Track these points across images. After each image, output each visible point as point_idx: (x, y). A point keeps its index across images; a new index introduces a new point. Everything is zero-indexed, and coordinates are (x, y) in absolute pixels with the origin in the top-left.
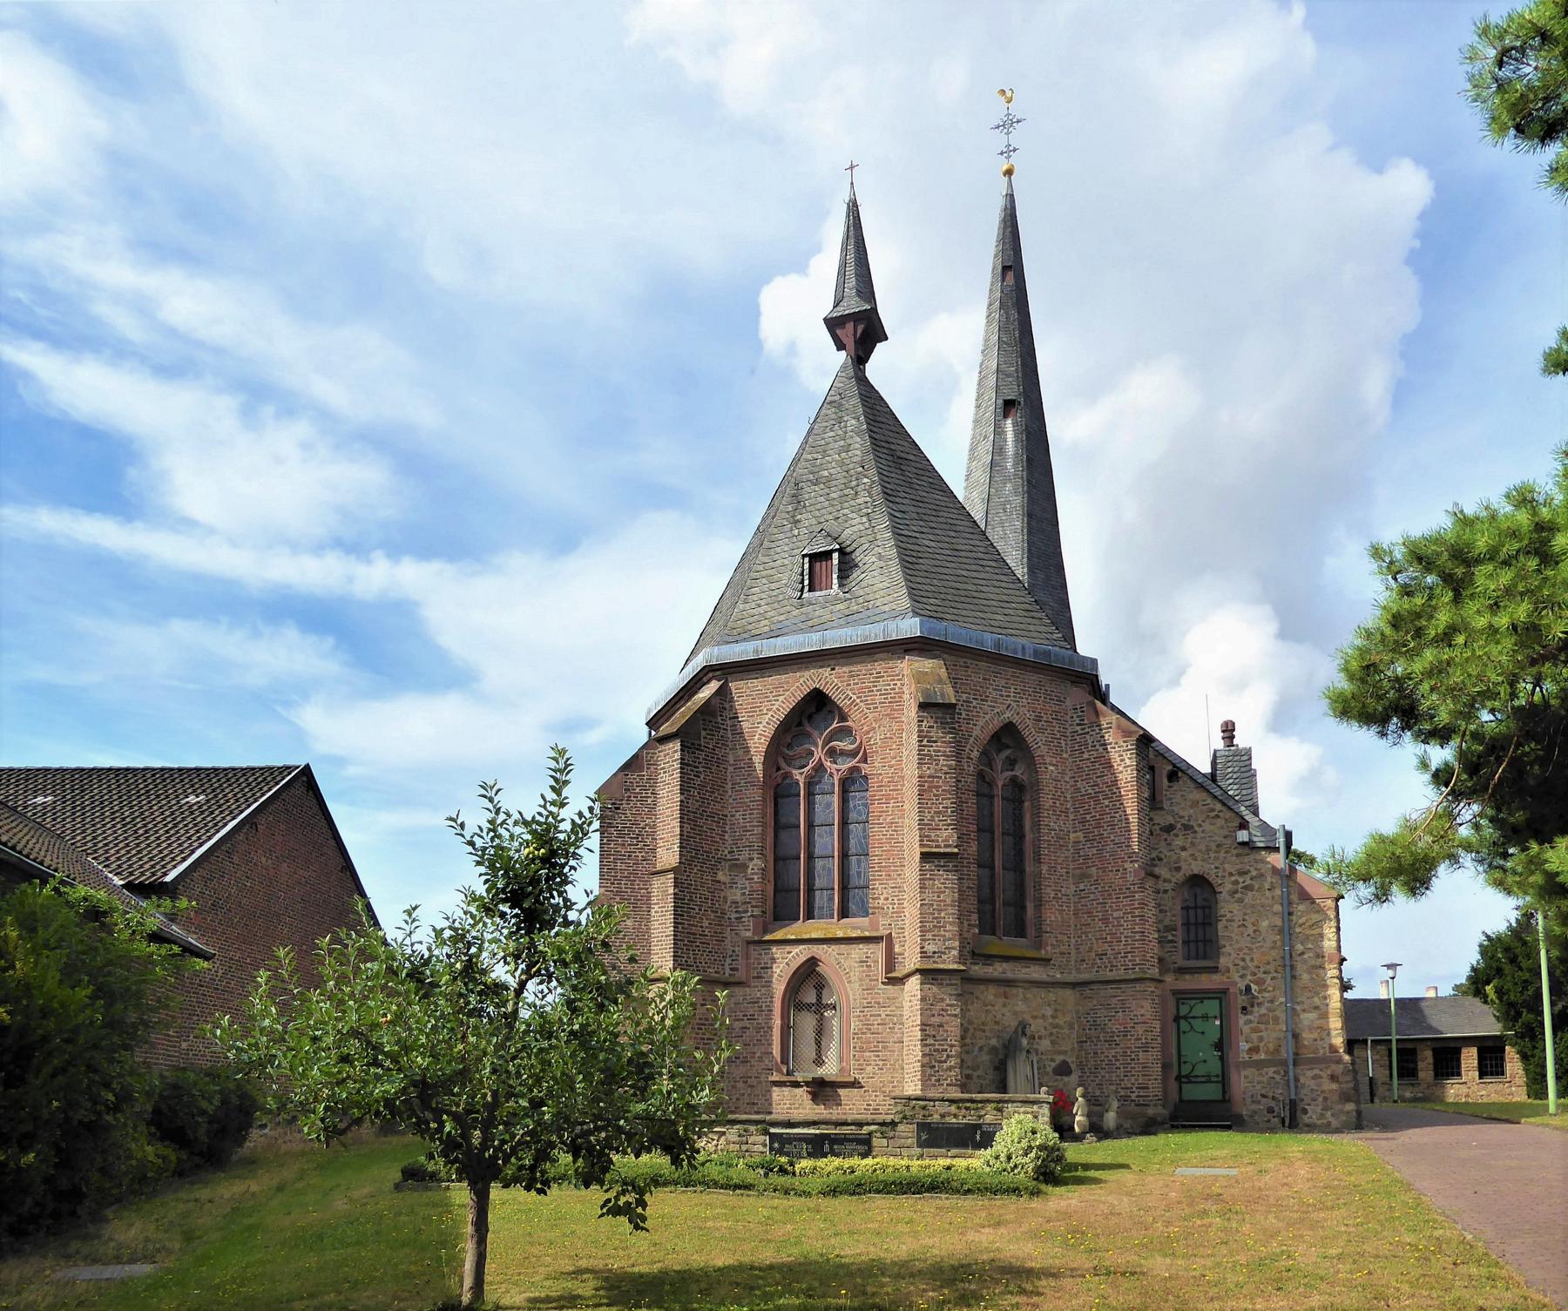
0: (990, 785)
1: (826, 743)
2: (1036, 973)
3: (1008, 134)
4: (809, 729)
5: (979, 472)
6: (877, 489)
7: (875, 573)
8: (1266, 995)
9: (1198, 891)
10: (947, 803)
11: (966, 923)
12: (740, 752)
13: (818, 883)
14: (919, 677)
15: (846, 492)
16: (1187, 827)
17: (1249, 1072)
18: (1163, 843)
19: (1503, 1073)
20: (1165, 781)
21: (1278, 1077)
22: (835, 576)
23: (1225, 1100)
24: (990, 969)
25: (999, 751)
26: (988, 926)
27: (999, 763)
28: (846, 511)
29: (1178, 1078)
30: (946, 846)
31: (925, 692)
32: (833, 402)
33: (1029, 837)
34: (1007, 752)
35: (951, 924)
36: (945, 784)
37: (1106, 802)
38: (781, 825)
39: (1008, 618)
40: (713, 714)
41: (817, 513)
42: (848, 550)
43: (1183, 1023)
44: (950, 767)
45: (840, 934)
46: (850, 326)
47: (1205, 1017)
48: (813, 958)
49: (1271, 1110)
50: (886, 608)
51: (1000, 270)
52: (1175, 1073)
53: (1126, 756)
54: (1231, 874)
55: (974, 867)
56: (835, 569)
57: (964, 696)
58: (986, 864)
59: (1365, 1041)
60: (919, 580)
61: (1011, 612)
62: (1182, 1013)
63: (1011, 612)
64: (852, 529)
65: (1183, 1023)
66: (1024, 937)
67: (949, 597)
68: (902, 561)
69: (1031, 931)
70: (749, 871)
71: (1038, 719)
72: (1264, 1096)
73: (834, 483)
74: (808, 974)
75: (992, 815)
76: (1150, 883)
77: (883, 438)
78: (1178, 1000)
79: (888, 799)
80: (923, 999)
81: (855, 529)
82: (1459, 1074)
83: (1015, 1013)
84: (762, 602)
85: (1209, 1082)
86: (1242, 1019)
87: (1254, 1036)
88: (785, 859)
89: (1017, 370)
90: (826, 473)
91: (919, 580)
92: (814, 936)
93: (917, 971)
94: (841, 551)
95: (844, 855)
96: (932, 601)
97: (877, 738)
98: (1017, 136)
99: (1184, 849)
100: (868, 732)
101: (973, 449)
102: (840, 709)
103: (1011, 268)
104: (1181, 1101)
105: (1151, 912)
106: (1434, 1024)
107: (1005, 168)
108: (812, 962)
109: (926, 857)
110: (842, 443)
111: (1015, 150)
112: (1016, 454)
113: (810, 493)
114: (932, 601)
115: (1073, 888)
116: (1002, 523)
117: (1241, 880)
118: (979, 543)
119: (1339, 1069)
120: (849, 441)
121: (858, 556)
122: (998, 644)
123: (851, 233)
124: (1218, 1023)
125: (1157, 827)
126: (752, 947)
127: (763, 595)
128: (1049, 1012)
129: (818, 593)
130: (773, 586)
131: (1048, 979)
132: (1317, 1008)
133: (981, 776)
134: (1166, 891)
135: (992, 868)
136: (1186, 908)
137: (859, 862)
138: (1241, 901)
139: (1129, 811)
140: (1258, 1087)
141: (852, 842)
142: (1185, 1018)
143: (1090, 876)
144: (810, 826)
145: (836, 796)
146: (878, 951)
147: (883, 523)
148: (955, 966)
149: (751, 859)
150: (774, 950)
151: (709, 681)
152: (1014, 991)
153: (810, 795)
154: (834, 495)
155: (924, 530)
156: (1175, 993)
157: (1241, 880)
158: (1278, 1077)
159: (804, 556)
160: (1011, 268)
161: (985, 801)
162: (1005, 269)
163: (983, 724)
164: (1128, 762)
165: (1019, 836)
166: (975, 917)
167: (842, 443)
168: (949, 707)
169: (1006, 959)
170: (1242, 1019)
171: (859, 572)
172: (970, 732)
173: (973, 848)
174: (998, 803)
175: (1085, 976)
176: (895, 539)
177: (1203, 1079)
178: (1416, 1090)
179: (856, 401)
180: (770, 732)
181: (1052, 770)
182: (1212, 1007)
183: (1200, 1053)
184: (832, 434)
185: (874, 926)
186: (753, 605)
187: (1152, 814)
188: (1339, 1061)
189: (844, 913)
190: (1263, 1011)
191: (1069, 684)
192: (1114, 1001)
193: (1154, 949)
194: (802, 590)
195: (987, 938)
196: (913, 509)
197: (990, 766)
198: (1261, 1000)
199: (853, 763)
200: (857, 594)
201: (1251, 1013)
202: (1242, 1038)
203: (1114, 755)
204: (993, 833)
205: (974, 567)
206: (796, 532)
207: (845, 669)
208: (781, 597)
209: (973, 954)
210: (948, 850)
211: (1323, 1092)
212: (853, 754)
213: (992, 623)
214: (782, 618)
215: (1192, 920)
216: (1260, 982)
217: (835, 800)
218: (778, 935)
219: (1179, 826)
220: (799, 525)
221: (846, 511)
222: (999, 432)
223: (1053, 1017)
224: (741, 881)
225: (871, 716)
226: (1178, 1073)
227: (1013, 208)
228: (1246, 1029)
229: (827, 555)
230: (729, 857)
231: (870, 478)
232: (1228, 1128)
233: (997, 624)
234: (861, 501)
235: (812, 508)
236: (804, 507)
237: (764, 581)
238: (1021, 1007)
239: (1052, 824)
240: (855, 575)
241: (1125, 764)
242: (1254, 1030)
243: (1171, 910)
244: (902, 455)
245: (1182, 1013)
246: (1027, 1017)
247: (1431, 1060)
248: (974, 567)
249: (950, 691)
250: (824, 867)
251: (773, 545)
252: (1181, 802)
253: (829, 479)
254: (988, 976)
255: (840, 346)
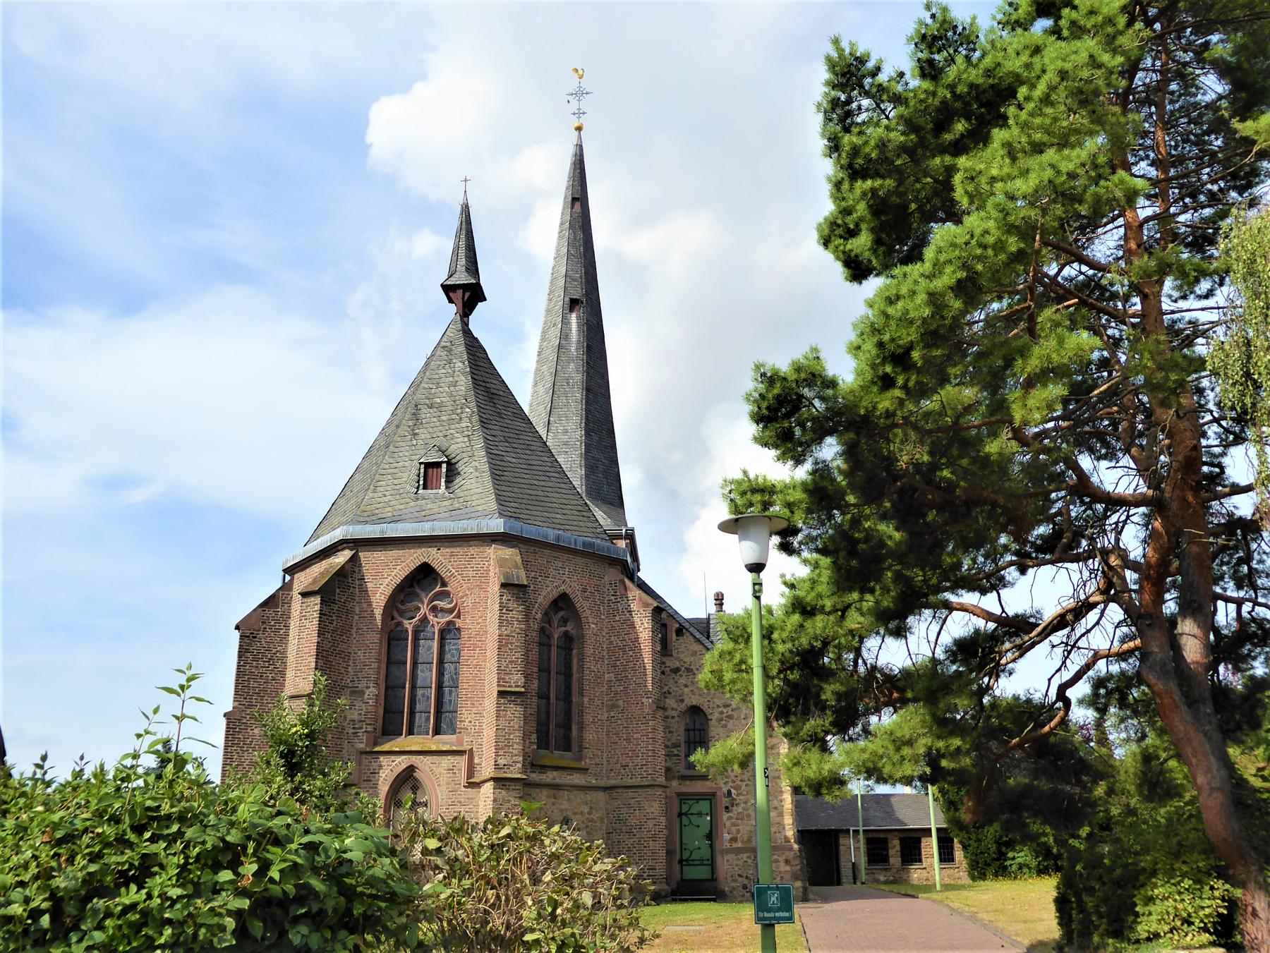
0: (549, 637)
1: (431, 601)
2: (577, 779)
3: (579, 109)
4: (418, 590)
5: (548, 352)
6: (476, 418)
7: (472, 481)
8: (742, 797)
9: (696, 717)
10: (518, 655)
11: (528, 741)
12: (365, 605)
13: (418, 708)
14: (501, 562)
15: (453, 416)
16: (688, 670)
17: (730, 857)
18: (671, 681)
19: (953, 860)
20: (674, 635)
21: (750, 861)
22: (443, 480)
23: (713, 879)
24: (543, 777)
25: (556, 612)
26: (543, 743)
27: (556, 620)
28: (452, 431)
29: (681, 861)
30: (517, 686)
31: (506, 575)
32: (443, 347)
33: (575, 676)
34: (562, 613)
35: (517, 744)
36: (517, 641)
37: (631, 653)
38: (392, 661)
39: (565, 517)
40: (345, 576)
41: (431, 430)
42: (454, 461)
43: (684, 818)
44: (521, 629)
45: (434, 748)
46: (460, 292)
47: (700, 814)
48: (412, 766)
49: (745, 887)
50: (479, 508)
51: (570, 198)
52: (678, 857)
53: (645, 621)
54: (718, 706)
55: (535, 699)
56: (444, 475)
57: (533, 574)
58: (543, 695)
59: (848, 831)
60: (504, 488)
61: (568, 512)
62: (684, 811)
63: (568, 512)
64: (457, 446)
65: (684, 818)
66: (570, 751)
67: (525, 501)
68: (493, 474)
69: (575, 747)
70: (366, 696)
71: (584, 591)
72: (740, 876)
73: (444, 409)
74: (407, 779)
75: (549, 658)
76: (660, 714)
77: (481, 378)
78: (681, 800)
79: (475, 646)
80: (495, 800)
81: (459, 446)
82: (920, 861)
83: (561, 810)
84: (387, 493)
85: (702, 865)
86: (725, 816)
87: (734, 829)
88: (393, 688)
89: (581, 277)
90: (438, 400)
91: (504, 488)
92: (414, 748)
93: (492, 779)
94: (449, 463)
95: (440, 687)
96: (512, 504)
97: (469, 602)
98: (586, 104)
99: (686, 686)
100: (462, 597)
101: (544, 332)
102: (442, 578)
103: (579, 199)
104: (682, 880)
105: (660, 735)
106: (901, 817)
107: (576, 125)
108: (411, 769)
109: (501, 694)
110: (451, 379)
111: (584, 113)
112: (579, 341)
113: (425, 413)
114: (512, 504)
115: (606, 715)
116: (566, 393)
117: (725, 711)
118: (546, 459)
119: (791, 855)
120: (456, 379)
121: (460, 466)
122: (558, 538)
123: (464, 227)
124: (709, 818)
125: (668, 669)
126: (364, 756)
127: (388, 488)
128: (586, 810)
129: (430, 491)
130: (396, 482)
131: (586, 784)
132: (776, 808)
133: (542, 630)
134: (673, 717)
135: (548, 699)
136: (687, 730)
137: (451, 692)
138: (725, 726)
139: (646, 661)
140: (736, 869)
141: (446, 677)
142: (686, 814)
143: (618, 707)
144: (415, 664)
145: (436, 641)
146: (462, 762)
147: (479, 444)
148: (519, 776)
149: (368, 687)
150: (382, 758)
151: (342, 550)
152: (561, 793)
153: (416, 639)
154: (444, 418)
155: (508, 449)
156: (679, 794)
157: (725, 711)
158: (750, 861)
159: (420, 463)
160: (579, 199)
161: (545, 674)
162: (574, 200)
163: (545, 594)
164: (646, 625)
165: (568, 675)
166: (534, 736)
167: (451, 379)
168: (522, 587)
169: (557, 768)
170: (725, 816)
171: (460, 479)
172: (536, 599)
173: (535, 685)
174: (554, 650)
175: (613, 782)
176: (488, 458)
177: (698, 862)
178: (889, 874)
179: (462, 349)
180: (389, 591)
181: (594, 627)
182: (704, 806)
183: (696, 842)
184: (444, 371)
185: (460, 742)
186: (380, 495)
187: (664, 659)
188: (791, 849)
189: (437, 731)
190: (740, 809)
191: (607, 566)
192: (632, 801)
193: (661, 763)
194: (418, 488)
195: (543, 752)
196: (501, 433)
197: (549, 623)
198: (738, 801)
199: (450, 618)
200: (459, 495)
201: (732, 811)
202: (725, 830)
203: (637, 620)
204: (549, 672)
205: (543, 478)
206: (414, 442)
207: (447, 550)
208: (401, 491)
209: (532, 765)
210: (518, 689)
211: (780, 872)
212: (451, 611)
213: (554, 520)
214: (402, 507)
215: (692, 740)
216: (737, 788)
217: (435, 645)
218: (386, 747)
219: (683, 669)
220: (417, 437)
221: (452, 431)
222: (565, 322)
223: (589, 813)
224: (358, 704)
225: (465, 586)
226: (678, 855)
227: (582, 156)
228: (728, 824)
229: (438, 465)
230: (350, 685)
231: (471, 409)
232: (714, 900)
233: (557, 521)
234: (464, 425)
235: (427, 426)
236: (422, 423)
237: (389, 477)
238: (565, 805)
239: (591, 666)
240: (457, 481)
241: (644, 626)
242: (734, 825)
243: (677, 731)
244: (495, 391)
245: (684, 811)
246: (570, 814)
247: (898, 848)
248: (543, 478)
249: (522, 573)
250: (423, 695)
251: (396, 450)
252: (684, 648)
253: (441, 405)
254: (543, 782)
255: (451, 301)
